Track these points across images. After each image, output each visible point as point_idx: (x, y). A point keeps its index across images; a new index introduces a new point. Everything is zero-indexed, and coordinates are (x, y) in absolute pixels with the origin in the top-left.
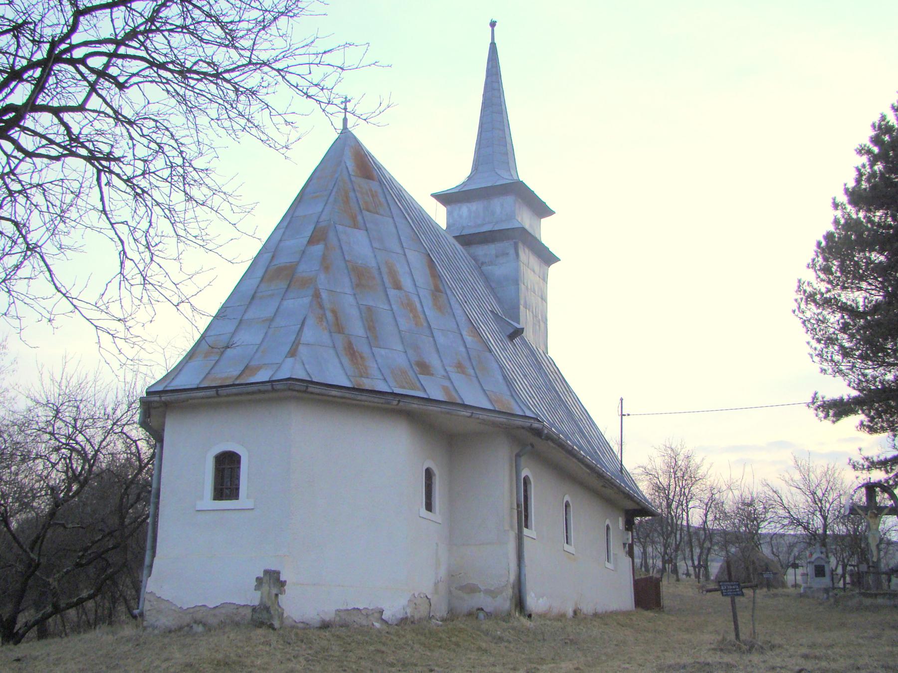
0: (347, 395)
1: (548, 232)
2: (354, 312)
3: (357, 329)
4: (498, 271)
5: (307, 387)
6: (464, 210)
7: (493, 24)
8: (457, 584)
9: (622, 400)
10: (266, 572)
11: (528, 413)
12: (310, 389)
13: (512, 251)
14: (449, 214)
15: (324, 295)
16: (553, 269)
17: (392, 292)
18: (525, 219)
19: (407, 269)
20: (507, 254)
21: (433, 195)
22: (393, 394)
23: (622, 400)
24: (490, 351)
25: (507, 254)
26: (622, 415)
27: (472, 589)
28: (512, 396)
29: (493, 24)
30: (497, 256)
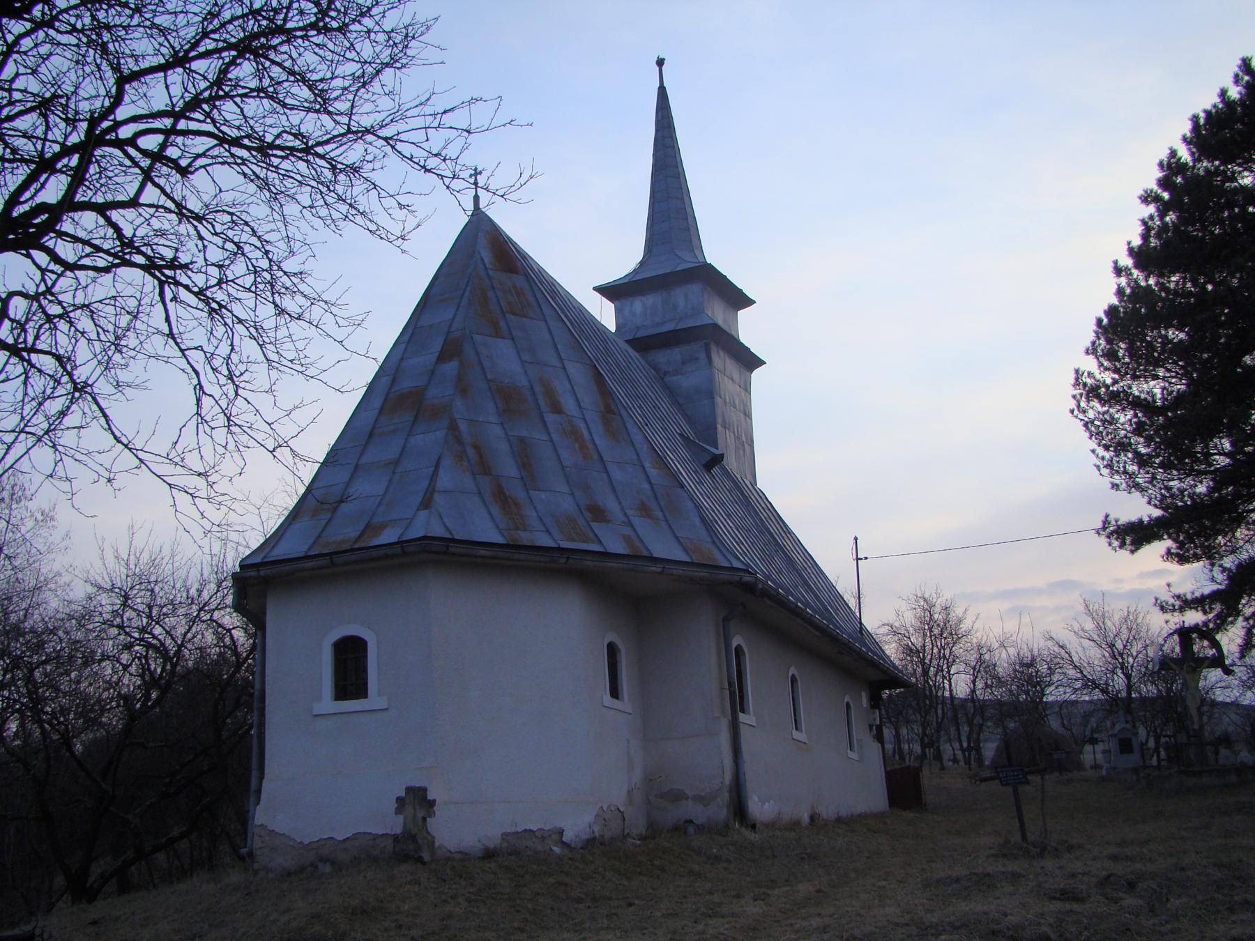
0: (500, 554)
1: (749, 328)
2: (503, 447)
3: (508, 467)
4: (687, 381)
5: (448, 547)
6: (637, 305)
7: (660, 63)
8: (657, 790)
9: (856, 539)
10: (409, 790)
11: (736, 564)
12: (452, 550)
13: (702, 356)
14: (618, 312)
15: (463, 427)
16: (757, 375)
17: (550, 418)
18: (716, 312)
19: (568, 386)
20: (697, 359)
21: (597, 289)
22: (559, 549)
23: (856, 539)
24: (682, 486)
25: (697, 359)
26: (858, 559)
27: (677, 797)
28: (714, 542)
29: (660, 63)
30: (683, 363)
